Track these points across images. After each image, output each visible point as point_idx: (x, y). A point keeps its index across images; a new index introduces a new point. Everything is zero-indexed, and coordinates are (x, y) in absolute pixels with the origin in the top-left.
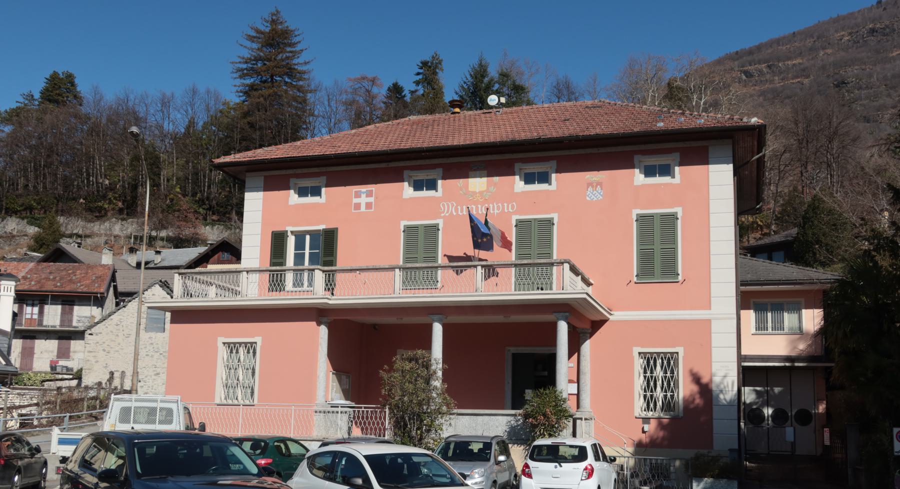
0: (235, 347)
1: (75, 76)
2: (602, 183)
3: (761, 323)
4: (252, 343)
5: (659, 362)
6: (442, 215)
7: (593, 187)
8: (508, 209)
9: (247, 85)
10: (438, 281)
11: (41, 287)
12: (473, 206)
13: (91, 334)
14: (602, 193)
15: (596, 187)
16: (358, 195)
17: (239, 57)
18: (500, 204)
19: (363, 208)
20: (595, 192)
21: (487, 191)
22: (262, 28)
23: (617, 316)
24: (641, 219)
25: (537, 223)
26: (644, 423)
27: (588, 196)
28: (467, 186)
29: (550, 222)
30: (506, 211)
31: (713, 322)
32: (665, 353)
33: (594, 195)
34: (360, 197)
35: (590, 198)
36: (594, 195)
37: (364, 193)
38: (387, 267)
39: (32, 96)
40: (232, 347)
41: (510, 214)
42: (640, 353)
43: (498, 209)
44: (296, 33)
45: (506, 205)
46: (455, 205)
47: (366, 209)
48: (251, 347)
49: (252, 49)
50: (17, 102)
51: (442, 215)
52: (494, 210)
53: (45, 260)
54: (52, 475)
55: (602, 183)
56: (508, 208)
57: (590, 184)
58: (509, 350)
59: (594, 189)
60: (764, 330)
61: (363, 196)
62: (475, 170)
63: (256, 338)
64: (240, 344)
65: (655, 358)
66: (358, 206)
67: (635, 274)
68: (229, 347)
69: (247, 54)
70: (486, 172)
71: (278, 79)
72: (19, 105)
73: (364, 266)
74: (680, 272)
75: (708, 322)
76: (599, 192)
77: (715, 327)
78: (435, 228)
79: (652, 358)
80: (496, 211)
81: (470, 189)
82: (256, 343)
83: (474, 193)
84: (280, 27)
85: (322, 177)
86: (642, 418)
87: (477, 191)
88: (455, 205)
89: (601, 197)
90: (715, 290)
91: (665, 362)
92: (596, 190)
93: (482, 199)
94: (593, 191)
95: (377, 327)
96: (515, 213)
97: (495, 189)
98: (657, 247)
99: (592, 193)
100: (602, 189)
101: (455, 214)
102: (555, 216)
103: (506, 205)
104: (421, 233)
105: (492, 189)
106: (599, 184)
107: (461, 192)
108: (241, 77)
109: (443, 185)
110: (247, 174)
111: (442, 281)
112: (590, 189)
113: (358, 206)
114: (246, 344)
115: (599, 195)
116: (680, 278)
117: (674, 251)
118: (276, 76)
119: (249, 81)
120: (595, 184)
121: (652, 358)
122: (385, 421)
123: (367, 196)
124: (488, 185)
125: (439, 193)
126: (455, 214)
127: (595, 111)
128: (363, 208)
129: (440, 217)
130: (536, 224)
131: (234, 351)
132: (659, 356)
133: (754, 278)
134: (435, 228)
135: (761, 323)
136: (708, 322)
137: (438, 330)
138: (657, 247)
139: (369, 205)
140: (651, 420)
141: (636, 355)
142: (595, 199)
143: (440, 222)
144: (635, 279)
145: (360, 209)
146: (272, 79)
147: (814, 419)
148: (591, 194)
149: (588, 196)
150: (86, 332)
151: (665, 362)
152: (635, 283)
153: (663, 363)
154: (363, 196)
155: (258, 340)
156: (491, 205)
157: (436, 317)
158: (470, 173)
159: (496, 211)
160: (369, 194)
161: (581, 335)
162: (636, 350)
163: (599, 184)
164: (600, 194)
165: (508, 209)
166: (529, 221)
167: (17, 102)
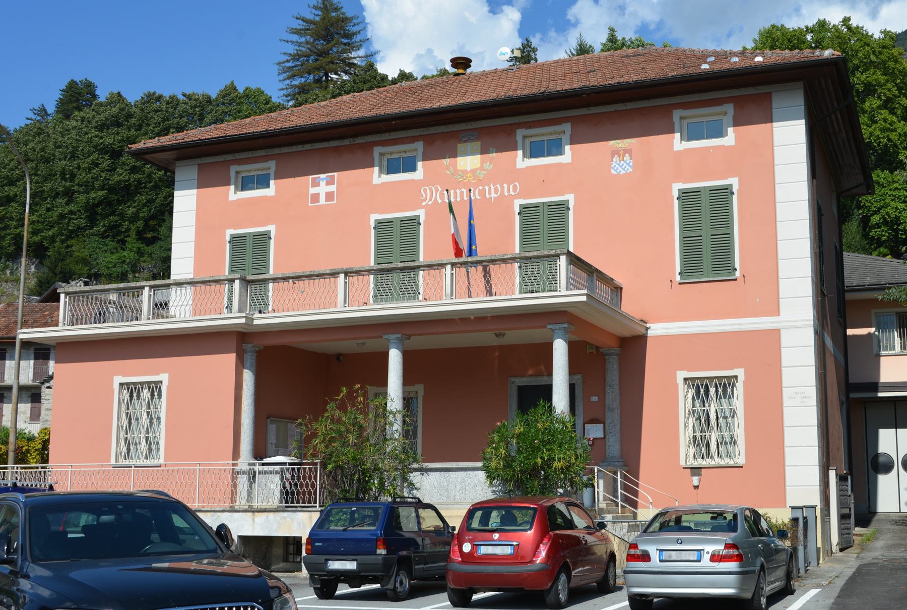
0: (156, 387)
1: (96, 84)
2: (631, 150)
3: (886, 340)
4: (156, 383)
5: (712, 390)
6: (424, 203)
7: (619, 156)
8: (509, 191)
9: (296, 86)
10: (419, 293)
11: (7, 333)
12: (463, 190)
13: (49, 388)
14: (631, 164)
15: (624, 155)
16: (316, 184)
17: (285, 54)
18: (498, 186)
19: (322, 200)
20: (622, 162)
21: (482, 168)
22: (310, 17)
23: (656, 330)
24: (686, 196)
25: (546, 207)
26: (693, 475)
27: (613, 168)
28: (455, 165)
29: (563, 207)
30: (506, 194)
31: (783, 333)
32: (720, 378)
33: (622, 166)
34: (318, 185)
35: (616, 171)
36: (621, 167)
37: (323, 180)
38: (328, 272)
39: (45, 110)
40: (133, 389)
41: (512, 198)
42: (686, 379)
43: (496, 192)
44: (355, 21)
45: (505, 185)
46: (440, 189)
47: (326, 201)
48: (155, 388)
49: (300, 44)
50: (28, 119)
51: (424, 203)
52: (490, 193)
53: (42, 301)
54: (899, 554)
55: (631, 150)
56: (509, 190)
57: (615, 153)
58: (513, 382)
59: (621, 158)
60: (890, 350)
61: (323, 183)
62: (465, 141)
63: (161, 375)
64: (142, 383)
65: (707, 385)
66: (316, 198)
67: (678, 270)
68: (128, 389)
69: (291, 49)
70: (477, 145)
71: (334, 76)
72: (28, 122)
73: (299, 271)
74: (737, 266)
75: (776, 333)
76: (628, 162)
77: (786, 338)
78: (415, 221)
79: (702, 385)
80: (493, 195)
81: (459, 167)
82: (161, 382)
83: (465, 172)
84: (334, 14)
85: (269, 162)
86: (691, 468)
87: (469, 170)
88: (440, 189)
89: (630, 170)
90: (785, 288)
91: (720, 390)
92: (623, 160)
93: (474, 179)
94: (620, 161)
95: (341, 358)
96: (518, 196)
97: (492, 165)
98: (706, 232)
99: (618, 164)
100: (631, 159)
101: (440, 201)
102: (570, 198)
103: (505, 185)
104: (396, 228)
105: (487, 166)
106: (628, 151)
107: (447, 172)
108: (289, 78)
109: (423, 167)
110: (178, 163)
111: (424, 291)
112: (616, 159)
113: (316, 198)
114: (149, 383)
115: (628, 167)
116: (738, 274)
117: (729, 235)
118: (331, 72)
119: (297, 82)
120: (622, 152)
121: (702, 385)
122: (316, 482)
123: (328, 184)
124: (482, 162)
125: (419, 174)
126: (440, 201)
127: (634, 59)
128: (322, 200)
129: (422, 207)
130: (546, 210)
131: (135, 395)
132: (711, 382)
133: (875, 281)
134: (415, 221)
135: (886, 340)
136: (776, 333)
137: (395, 358)
138: (706, 232)
139: (329, 196)
140: (702, 470)
141: (680, 382)
142: (623, 172)
143: (421, 213)
144: (678, 278)
145: (319, 202)
146: (327, 76)
147: (870, 460)
148: (617, 166)
149: (613, 168)
150: (43, 387)
151: (720, 390)
152: (680, 284)
153: (717, 391)
154: (323, 183)
155: (164, 378)
156: (487, 188)
157: (392, 337)
158: (461, 147)
159: (493, 195)
160: (330, 182)
161: (607, 357)
162: (681, 375)
163: (628, 151)
164: (628, 164)
165: (509, 191)
166: (536, 206)
167: (28, 119)
